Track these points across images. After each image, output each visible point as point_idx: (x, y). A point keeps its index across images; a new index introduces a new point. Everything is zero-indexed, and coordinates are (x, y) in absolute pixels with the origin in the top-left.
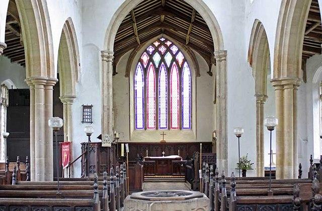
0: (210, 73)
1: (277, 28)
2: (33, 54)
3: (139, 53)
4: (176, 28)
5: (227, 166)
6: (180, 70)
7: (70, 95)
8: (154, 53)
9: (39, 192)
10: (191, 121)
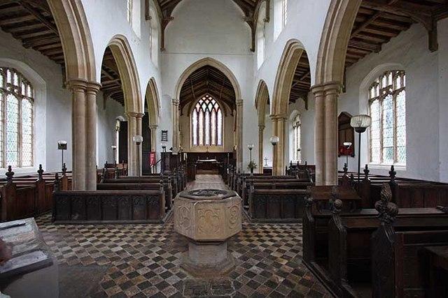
0: (232, 115)
1: (321, 43)
4: (212, 88)
5: (243, 166)
6: (217, 114)
10: (222, 141)
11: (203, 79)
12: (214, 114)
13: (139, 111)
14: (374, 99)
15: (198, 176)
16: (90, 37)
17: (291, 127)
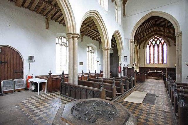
4: (160, 31)
6: (163, 45)
7: (120, 53)
8: (153, 41)
9: (47, 88)
10: (167, 61)
11: (152, 26)
12: (156, 47)
13: (108, 46)
15: (35, 86)
16: (73, 12)
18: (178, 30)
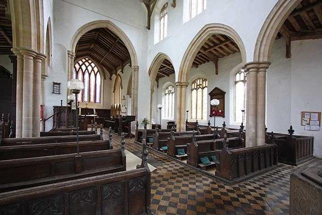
2: (23, 27)
3: (78, 60)
4: (97, 53)
8: (82, 65)
10: (100, 99)
12: (87, 75)
14: (238, 82)
17: (163, 94)
18: (135, 63)
